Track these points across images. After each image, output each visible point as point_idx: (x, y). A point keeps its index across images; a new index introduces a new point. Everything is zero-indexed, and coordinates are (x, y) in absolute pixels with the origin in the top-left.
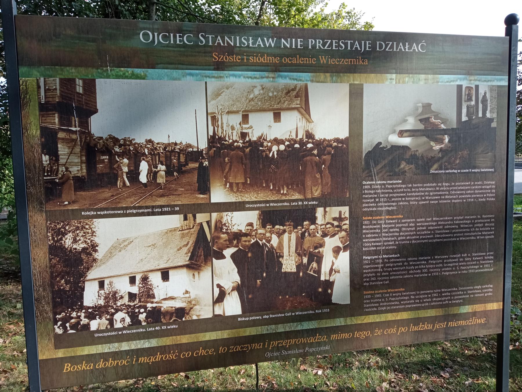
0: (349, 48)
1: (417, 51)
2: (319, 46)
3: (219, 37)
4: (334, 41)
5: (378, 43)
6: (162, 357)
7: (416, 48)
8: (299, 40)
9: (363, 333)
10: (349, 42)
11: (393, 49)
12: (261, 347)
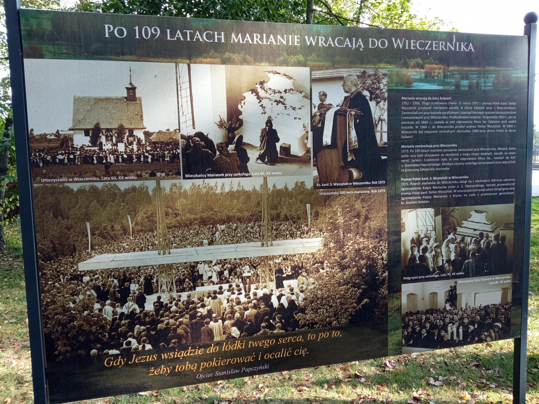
0: (189, 39)
1: (333, 46)
2: (322, 43)
3: (360, 40)
4: (434, 42)
5: (370, 39)
6: (230, 361)
7: (332, 43)
8: (296, 37)
9: (267, 342)
10: (188, 32)
11: (432, 48)
12: (202, 364)
